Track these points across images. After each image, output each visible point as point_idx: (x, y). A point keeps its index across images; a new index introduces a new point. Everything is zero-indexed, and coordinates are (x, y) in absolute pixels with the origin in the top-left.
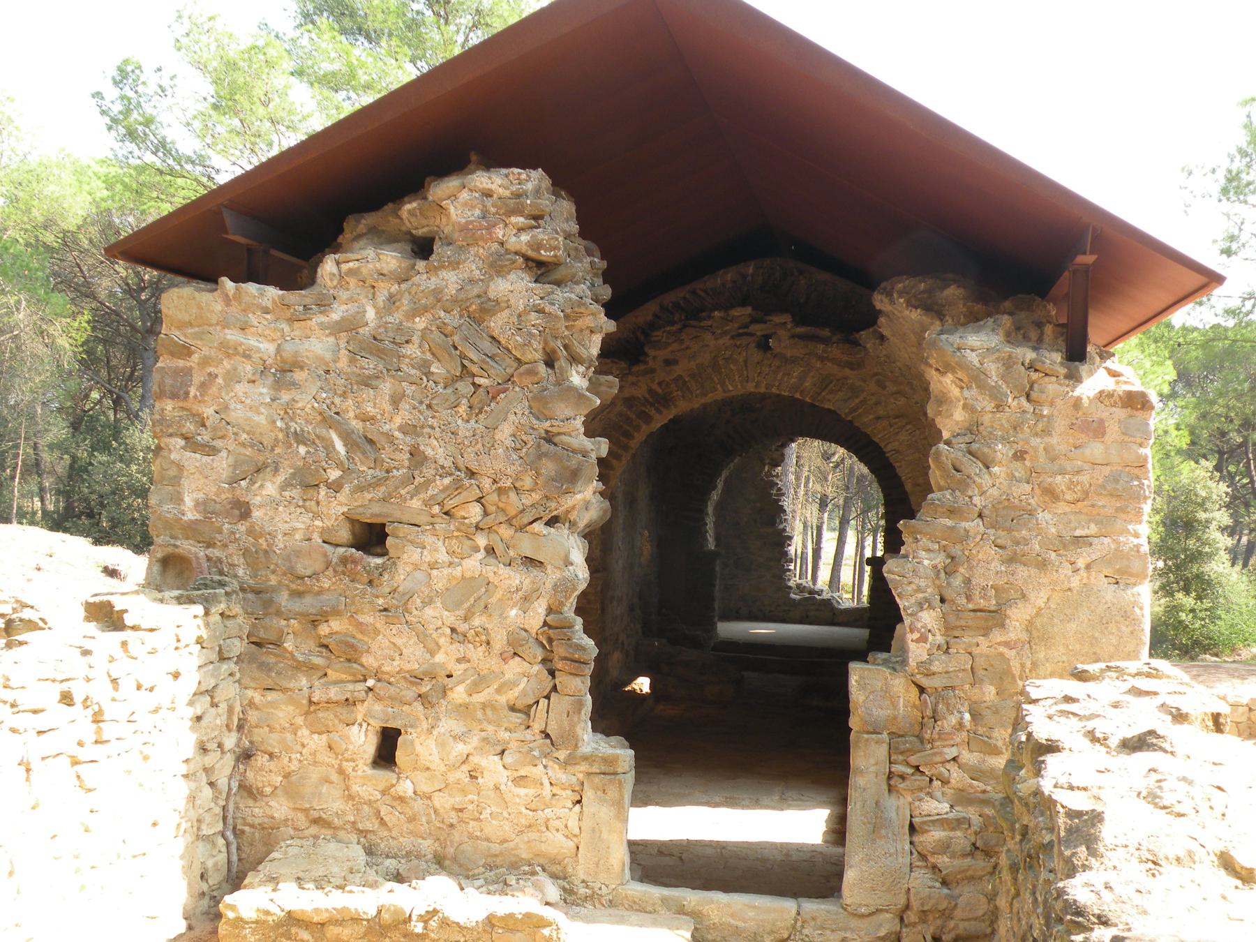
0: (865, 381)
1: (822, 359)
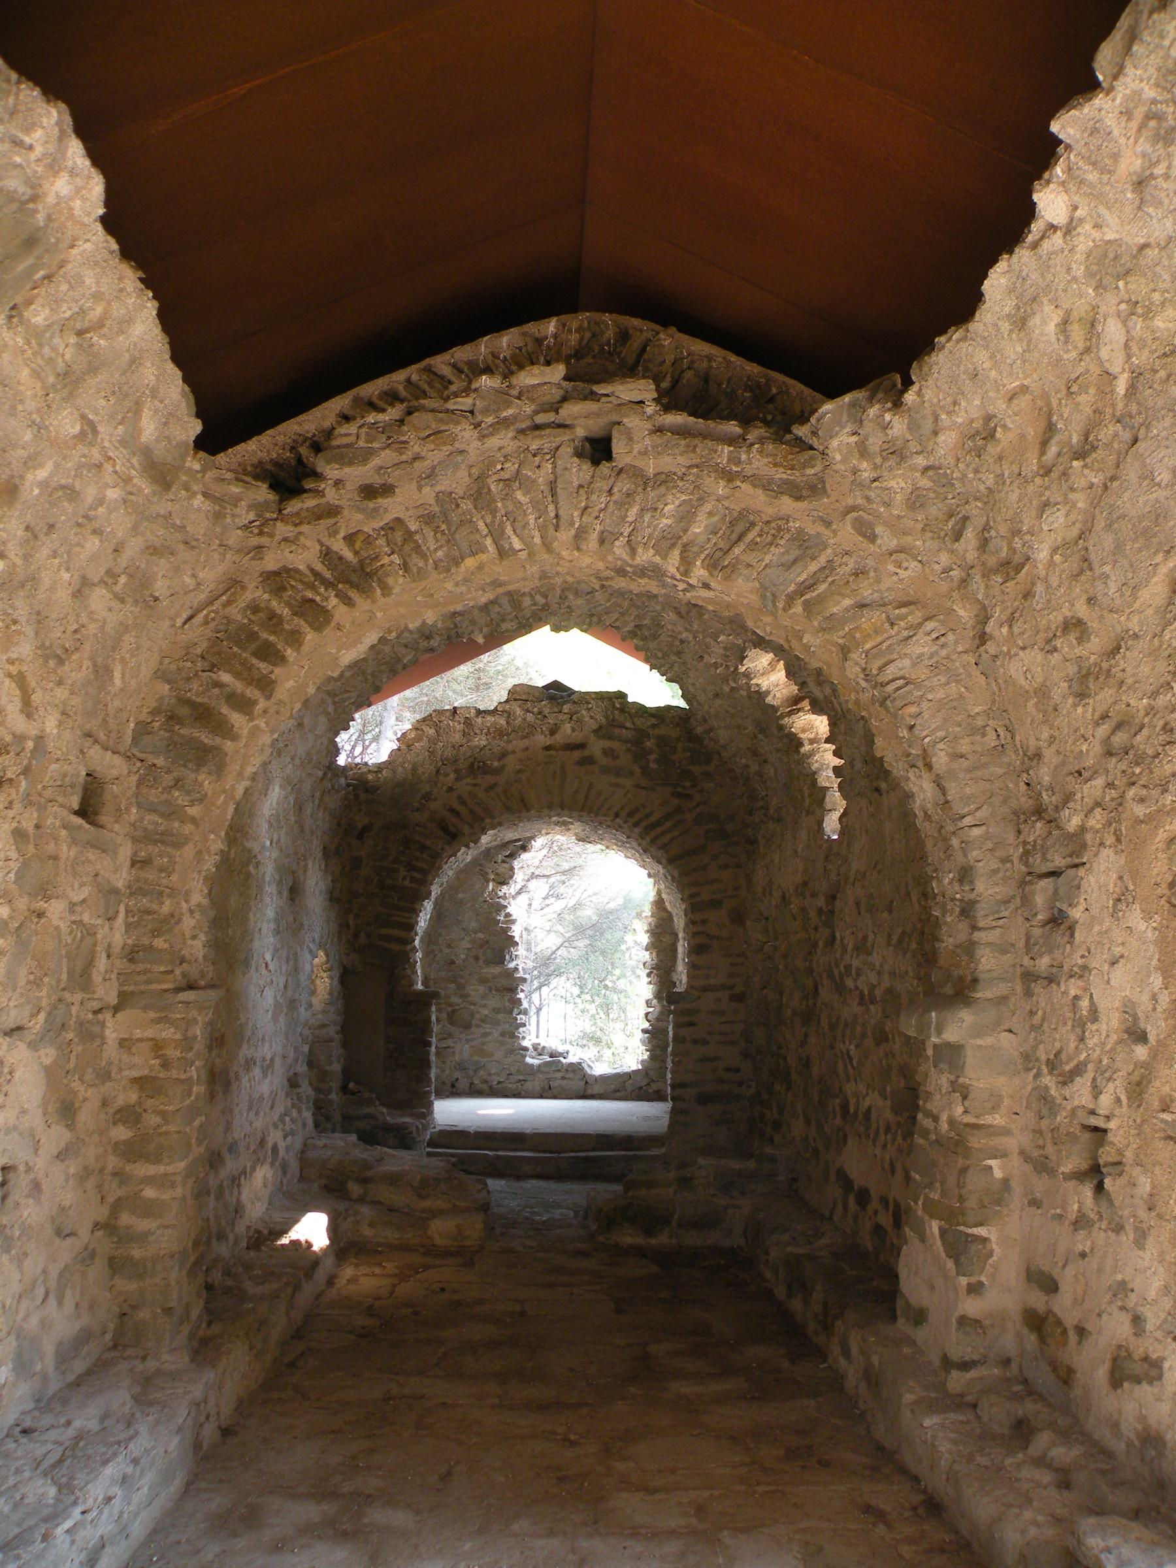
0: (828, 524)
1: (729, 477)
